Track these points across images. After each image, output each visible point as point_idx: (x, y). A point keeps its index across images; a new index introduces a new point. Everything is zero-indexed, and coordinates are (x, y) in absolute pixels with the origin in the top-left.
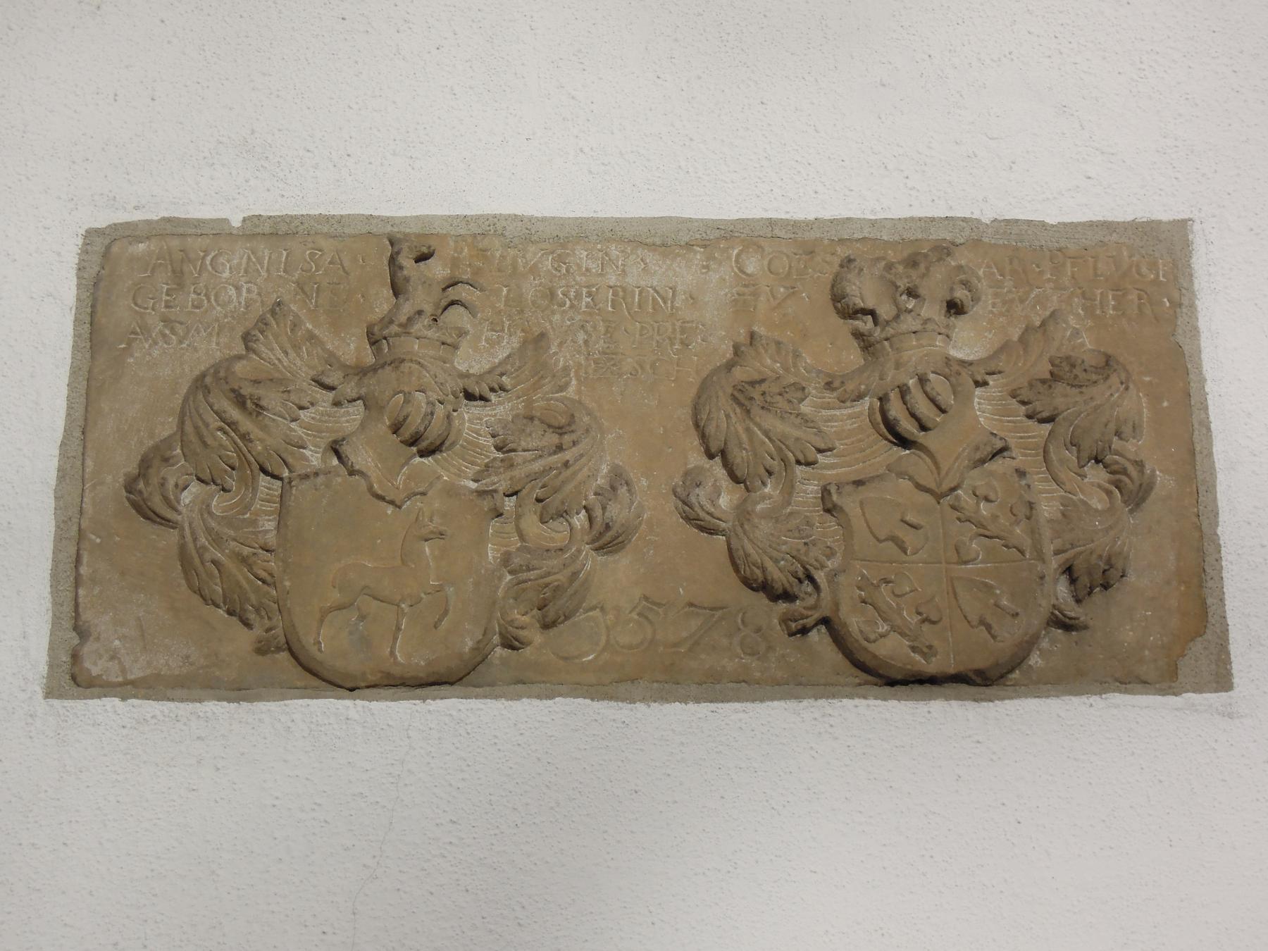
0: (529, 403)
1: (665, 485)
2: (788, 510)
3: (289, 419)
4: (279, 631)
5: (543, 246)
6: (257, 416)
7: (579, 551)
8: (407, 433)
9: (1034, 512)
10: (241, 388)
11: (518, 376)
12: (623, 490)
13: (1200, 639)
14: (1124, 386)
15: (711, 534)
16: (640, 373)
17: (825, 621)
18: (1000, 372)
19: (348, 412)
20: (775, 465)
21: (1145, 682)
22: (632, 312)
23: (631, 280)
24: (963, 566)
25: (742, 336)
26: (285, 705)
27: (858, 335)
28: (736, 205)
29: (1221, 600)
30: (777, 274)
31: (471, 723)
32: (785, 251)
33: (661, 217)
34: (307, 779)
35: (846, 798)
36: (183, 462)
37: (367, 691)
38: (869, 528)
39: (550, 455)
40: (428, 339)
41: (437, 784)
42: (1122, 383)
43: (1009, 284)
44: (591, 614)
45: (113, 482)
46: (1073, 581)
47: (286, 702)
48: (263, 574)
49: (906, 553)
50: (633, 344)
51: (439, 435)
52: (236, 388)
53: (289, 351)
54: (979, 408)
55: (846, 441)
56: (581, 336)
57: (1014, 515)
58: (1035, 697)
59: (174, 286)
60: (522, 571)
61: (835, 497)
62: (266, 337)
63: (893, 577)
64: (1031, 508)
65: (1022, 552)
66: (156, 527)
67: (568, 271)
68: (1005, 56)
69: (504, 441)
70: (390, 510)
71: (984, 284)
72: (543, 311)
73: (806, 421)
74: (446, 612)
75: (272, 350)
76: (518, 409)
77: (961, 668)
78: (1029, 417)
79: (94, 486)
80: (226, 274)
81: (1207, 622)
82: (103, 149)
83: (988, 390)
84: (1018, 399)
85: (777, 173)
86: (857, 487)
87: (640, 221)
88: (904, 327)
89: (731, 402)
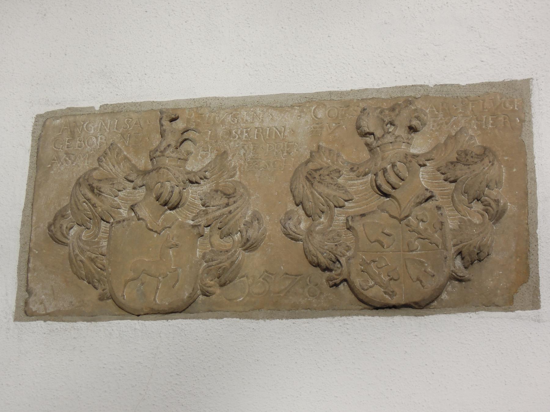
0: (217, 183)
1: (277, 219)
2: (330, 229)
3: (113, 195)
4: (107, 291)
5: (227, 110)
6: (99, 196)
7: (236, 251)
8: (162, 200)
9: (443, 227)
10: (93, 184)
11: (213, 172)
12: (256, 223)
13: (525, 284)
14: (491, 163)
15: (296, 241)
16: (268, 167)
17: (345, 280)
18: (432, 159)
19: (139, 191)
20: (325, 208)
21: (497, 306)
22: (265, 139)
23: (265, 124)
24: (411, 253)
25: (315, 148)
26: (110, 323)
27: (367, 145)
28: (314, 86)
29: (537, 265)
30: (332, 117)
31: (187, 330)
32: (336, 106)
33: (280, 94)
34: (118, 356)
35: (353, 363)
36: (71, 216)
37: (145, 316)
38: (367, 237)
39: (224, 208)
40: (173, 157)
41: (171, 358)
42: (490, 162)
43: (441, 115)
44: (242, 279)
45: (44, 226)
46: (463, 259)
47: (110, 322)
48: (100, 266)
49: (384, 248)
50: (265, 154)
51: (176, 201)
52: (91, 183)
53: (115, 165)
54: (422, 177)
55: (359, 195)
56: (242, 152)
57: (435, 228)
58: (444, 314)
59: (71, 138)
60: (210, 261)
61: (350, 223)
62: (106, 160)
63: (377, 259)
64: (442, 225)
65: (437, 246)
66: (60, 245)
67: (238, 121)
68: (445, 5)
69: (204, 202)
70: (155, 235)
71: (429, 116)
72: (226, 141)
73: (339, 187)
74: (177, 281)
75: (108, 165)
76: (212, 187)
77: (407, 302)
78: (445, 180)
79: (36, 228)
80: (92, 132)
81: (529, 276)
82: (44, 78)
83: (427, 168)
84: (440, 172)
85: (334, 69)
86: (362, 217)
87: (271, 96)
88: (386, 140)
89: (305, 180)
